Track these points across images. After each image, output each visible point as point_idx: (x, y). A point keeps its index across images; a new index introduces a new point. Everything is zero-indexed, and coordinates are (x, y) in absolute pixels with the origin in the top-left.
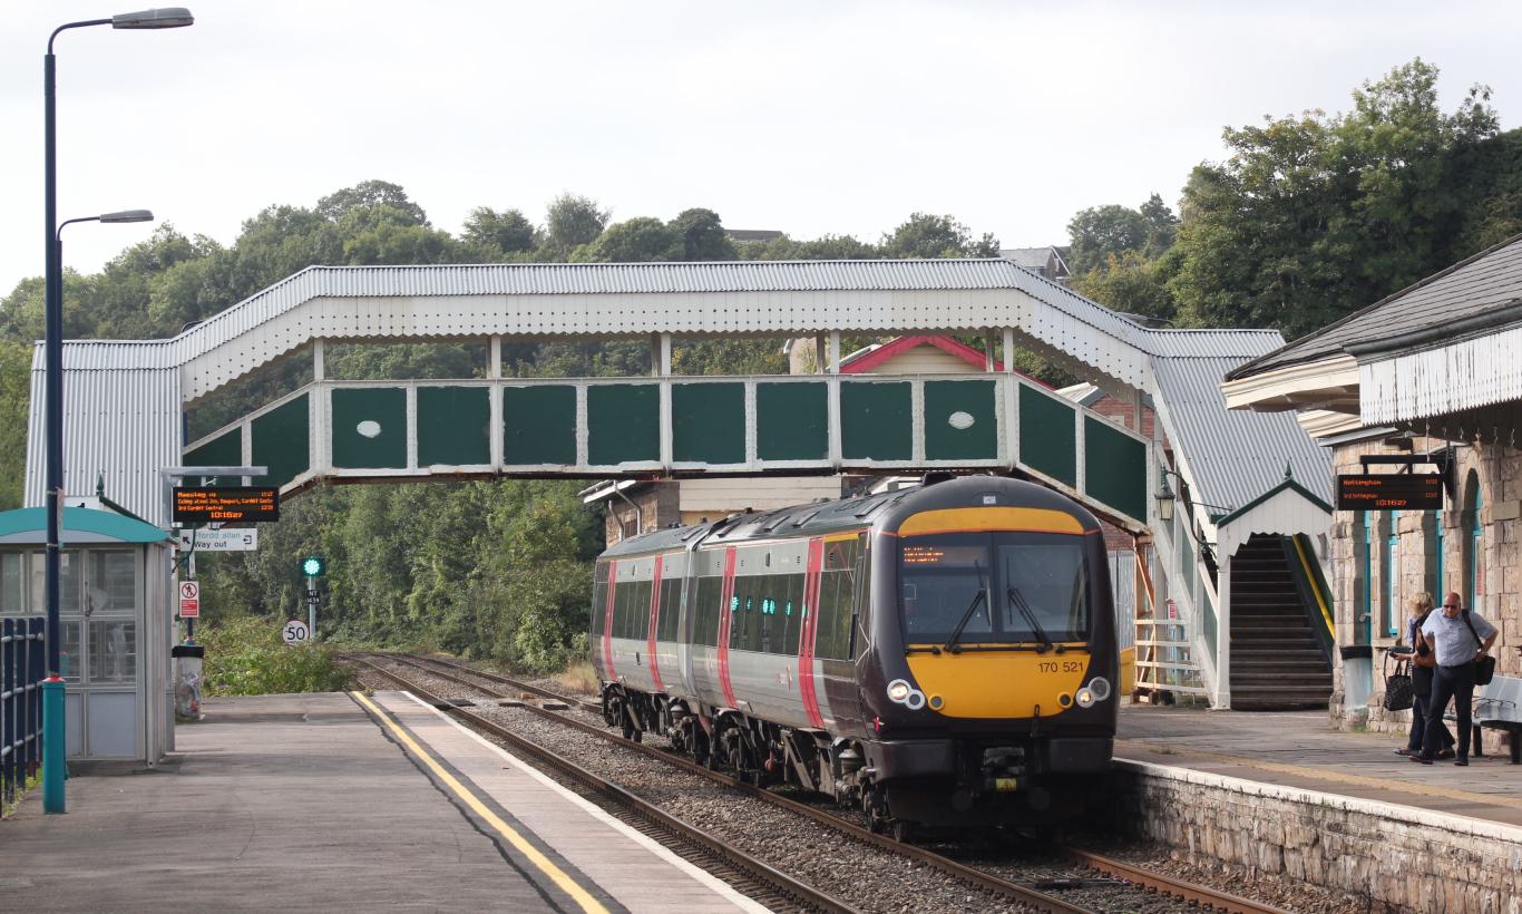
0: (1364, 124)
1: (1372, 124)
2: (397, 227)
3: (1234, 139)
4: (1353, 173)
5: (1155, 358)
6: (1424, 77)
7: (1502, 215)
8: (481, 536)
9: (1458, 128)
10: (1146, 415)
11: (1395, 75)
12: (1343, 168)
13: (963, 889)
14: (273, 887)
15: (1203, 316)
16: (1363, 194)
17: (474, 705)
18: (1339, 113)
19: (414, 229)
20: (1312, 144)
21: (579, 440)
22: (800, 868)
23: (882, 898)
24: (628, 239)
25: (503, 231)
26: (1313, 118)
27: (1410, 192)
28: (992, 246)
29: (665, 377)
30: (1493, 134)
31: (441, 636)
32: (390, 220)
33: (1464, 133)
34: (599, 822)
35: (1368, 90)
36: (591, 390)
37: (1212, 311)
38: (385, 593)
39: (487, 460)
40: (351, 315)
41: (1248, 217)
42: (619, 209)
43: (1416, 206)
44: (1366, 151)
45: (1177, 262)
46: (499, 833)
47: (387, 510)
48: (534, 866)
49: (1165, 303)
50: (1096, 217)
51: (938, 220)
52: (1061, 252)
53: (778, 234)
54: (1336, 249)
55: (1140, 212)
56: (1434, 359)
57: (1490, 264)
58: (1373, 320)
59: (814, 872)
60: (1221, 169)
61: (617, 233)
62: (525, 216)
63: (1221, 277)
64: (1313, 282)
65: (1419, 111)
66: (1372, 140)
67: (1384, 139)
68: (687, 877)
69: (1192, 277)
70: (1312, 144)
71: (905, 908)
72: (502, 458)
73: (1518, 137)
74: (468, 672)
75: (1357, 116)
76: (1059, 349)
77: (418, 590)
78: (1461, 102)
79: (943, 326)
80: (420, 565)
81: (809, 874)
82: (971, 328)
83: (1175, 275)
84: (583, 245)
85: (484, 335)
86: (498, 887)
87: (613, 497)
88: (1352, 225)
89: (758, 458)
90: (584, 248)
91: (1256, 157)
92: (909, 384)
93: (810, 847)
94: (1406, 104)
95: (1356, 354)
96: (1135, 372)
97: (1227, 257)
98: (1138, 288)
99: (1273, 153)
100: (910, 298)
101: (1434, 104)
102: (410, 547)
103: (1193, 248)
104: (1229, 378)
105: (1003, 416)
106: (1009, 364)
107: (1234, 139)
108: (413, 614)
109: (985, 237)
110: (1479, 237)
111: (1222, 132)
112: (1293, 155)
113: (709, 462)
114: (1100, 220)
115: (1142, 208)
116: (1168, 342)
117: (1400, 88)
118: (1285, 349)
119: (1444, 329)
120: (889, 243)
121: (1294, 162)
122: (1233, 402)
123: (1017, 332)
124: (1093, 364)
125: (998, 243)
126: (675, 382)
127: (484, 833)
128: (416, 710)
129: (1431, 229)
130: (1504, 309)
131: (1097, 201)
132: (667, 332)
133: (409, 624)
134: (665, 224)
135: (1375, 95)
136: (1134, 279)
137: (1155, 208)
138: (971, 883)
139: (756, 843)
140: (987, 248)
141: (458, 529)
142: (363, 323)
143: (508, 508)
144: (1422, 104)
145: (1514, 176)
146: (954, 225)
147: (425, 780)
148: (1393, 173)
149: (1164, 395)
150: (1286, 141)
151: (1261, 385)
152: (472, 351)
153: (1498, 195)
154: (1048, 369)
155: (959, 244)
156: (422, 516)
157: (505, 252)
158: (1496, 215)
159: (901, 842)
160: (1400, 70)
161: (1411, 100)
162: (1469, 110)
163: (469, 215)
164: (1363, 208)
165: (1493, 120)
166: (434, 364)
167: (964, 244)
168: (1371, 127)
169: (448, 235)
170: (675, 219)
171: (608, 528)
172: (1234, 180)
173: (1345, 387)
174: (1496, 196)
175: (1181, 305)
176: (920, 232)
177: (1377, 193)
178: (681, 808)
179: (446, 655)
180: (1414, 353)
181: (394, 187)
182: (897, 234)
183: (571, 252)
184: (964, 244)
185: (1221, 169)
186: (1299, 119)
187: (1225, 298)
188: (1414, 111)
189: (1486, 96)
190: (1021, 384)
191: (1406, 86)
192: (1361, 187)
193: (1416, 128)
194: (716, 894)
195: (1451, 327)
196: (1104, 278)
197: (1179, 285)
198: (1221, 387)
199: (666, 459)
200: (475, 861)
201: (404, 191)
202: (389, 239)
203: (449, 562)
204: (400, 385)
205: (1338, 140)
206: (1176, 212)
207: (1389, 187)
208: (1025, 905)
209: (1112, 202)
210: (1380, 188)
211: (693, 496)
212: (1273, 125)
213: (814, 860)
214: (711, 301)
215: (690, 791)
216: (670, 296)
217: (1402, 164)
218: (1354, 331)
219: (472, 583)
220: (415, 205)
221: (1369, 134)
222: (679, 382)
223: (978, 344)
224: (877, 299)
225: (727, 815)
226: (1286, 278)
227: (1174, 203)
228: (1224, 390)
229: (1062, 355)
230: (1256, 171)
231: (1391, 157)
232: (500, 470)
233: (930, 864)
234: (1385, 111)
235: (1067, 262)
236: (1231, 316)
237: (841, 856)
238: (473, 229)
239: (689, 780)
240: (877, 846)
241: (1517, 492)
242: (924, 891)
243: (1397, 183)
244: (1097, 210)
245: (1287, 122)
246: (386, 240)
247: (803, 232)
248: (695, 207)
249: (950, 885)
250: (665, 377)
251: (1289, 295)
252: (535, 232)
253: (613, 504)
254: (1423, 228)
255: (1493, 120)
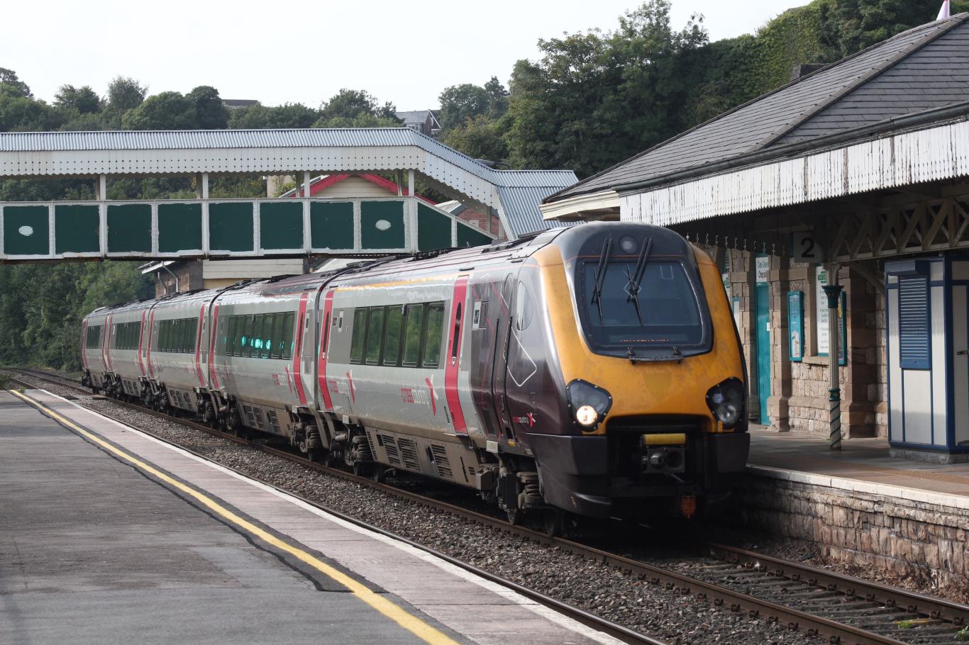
0: (625, 37)
1: (630, 37)
2: (12, 98)
3: (544, 46)
4: (619, 67)
5: (499, 188)
6: (662, 9)
7: (710, 94)
8: (72, 294)
9: (683, 40)
10: (494, 220)
11: (645, 7)
12: (612, 65)
13: (392, 500)
14: (24, 491)
15: (525, 156)
16: (624, 81)
17: (77, 399)
18: (610, 30)
19: (21, 99)
20: (593, 49)
21: (153, 237)
22: (295, 489)
23: (346, 504)
24: (160, 105)
25: (79, 100)
26: (594, 33)
27: (653, 76)
28: (391, 110)
29: (205, 200)
30: (705, 44)
31: (47, 357)
32: (6, 93)
33: (687, 43)
34: (189, 459)
35: (628, 16)
36: (161, 208)
37: (532, 153)
38: (9, 330)
39: (98, 250)
40: (15, 162)
41: (554, 94)
42: (154, 86)
43: (657, 89)
44: (626, 54)
45: (509, 123)
46: (135, 464)
47: (11, 278)
48: (162, 480)
49: (502, 148)
50: (457, 91)
51: (357, 94)
52: (435, 113)
53: (254, 102)
54: (608, 116)
55: (484, 88)
56: (662, 194)
57: (697, 136)
58: (628, 169)
59: (304, 491)
60: (537, 65)
61: (153, 101)
62: (93, 90)
63: (537, 132)
64: (594, 136)
65: (658, 32)
66: (631, 47)
67: (638, 46)
68: (249, 485)
69: (518, 133)
70: (593, 49)
71: (360, 509)
72: (107, 248)
73: (721, 46)
74: (67, 379)
75: (621, 32)
76: (448, 185)
77: (30, 329)
78: (685, 24)
79: (372, 168)
80: (32, 312)
81: (301, 492)
82: (389, 170)
83: (508, 131)
84: (131, 109)
85: (96, 174)
86: (148, 489)
87: (160, 270)
88: (617, 100)
89: (261, 248)
90: (132, 111)
91: (557, 57)
92: (352, 203)
93: (299, 477)
94: (651, 25)
95: (618, 191)
96: (487, 196)
97: (541, 120)
98: (486, 138)
99: (569, 55)
100: (352, 152)
101: (669, 25)
102: (25, 301)
103: (520, 110)
104: (545, 202)
105: (408, 223)
106: (411, 191)
107: (544, 46)
108: (27, 344)
109: (387, 104)
110: (696, 108)
111: (537, 42)
112: (581, 57)
113: (232, 250)
114: (459, 93)
115: (486, 85)
116: (508, 178)
117: (648, 15)
118: (577, 185)
119: (668, 178)
120: (326, 108)
121: (582, 60)
122: (547, 216)
123: (417, 172)
124: (462, 191)
125: (395, 108)
126: (210, 202)
127: (127, 465)
128: (53, 400)
129: (667, 103)
130: (700, 167)
131: (457, 82)
132: (206, 172)
133: (25, 350)
134: (184, 96)
135: (632, 19)
136: (482, 133)
137: (494, 85)
138: (396, 497)
139: (267, 476)
140: (388, 111)
141: (57, 290)
142: (22, 167)
143: (89, 276)
144: (661, 24)
145: (718, 70)
146: (367, 96)
147: (78, 438)
148: (644, 68)
149: (505, 209)
150: (577, 48)
151: (563, 206)
152: (87, 183)
153: (708, 81)
154: (430, 189)
155: (370, 109)
156: (33, 281)
157: (81, 114)
158: (706, 94)
159: (358, 475)
160: (647, 4)
161: (654, 22)
162: (691, 29)
163: (58, 90)
164: (624, 89)
165: (705, 35)
166: (36, 185)
167: (373, 109)
168: (629, 39)
169: (45, 102)
170: (190, 92)
171: (157, 289)
172: (546, 72)
173: (613, 208)
174: (707, 82)
175: (512, 149)
176: (346, 101)
177: (633, 80)
178: (218, 457)
179: (50, 369)
180: (651, 191)
181: (9, 71)
182: (331, 102)
183: (124, 113)
184: (373, 109)
185: (537, 65)
186: (585, 34)
187: (539, 145)
188: (655, 30)
189: (701, 20)
190: (419, 204)
191: (651, 13)
192: (623, 76)
193: (657, 40)
194: (267, 493)
195: (672, 176)
196: (464, 133)
197: (510, 137)
198: (539, 208)
199: (206, 248)
200: (129, 478)
201: (16, 75)
202: (8, 106)
203: (51, 310)
204: (45, 204)
205: (609, 47)
206: (507, 88)
207: (641, 76)
208: (428, 507)
209: (467, 83)
210: (635, 78)
211: (211, 270)
212: (569, 38)
213: (303, 484)
214: (232, 154)
215: (222, 447)
216: (208, 151)
217: (649, 62)
218: (617, 175)
219: (66, 324)
220: (23, 83)
221: (628, 43)
222: (213, 202)
223: (390, 179)
224: (333, 152)
225: (247, 461)
226: (577, 133)
227: (505, 82)
228: (541, 209)
229: (437, 182)
230: (558, 65)
231: (642, 58)
232: (105, 255)
233: (371, 486)
234: (639, 29)
235: (438, 120)
236: (543, 156)
237: (318, 482)
238: (61, 98)
239: (219, 441)
240: (338, 477)
241: (593, 290)
242: (369, 500)
243: (646, 74)
244: (457, 87)
245: (578, 36)
246: (6, 107)
247: (272, 99)
248: (202, 85)
249: (384, 497)
250: (205, 200)
251: (578, 144)
252: (100, 101)
253: (160, 275)
254: (661, 102)
255: (705, 35)
